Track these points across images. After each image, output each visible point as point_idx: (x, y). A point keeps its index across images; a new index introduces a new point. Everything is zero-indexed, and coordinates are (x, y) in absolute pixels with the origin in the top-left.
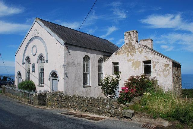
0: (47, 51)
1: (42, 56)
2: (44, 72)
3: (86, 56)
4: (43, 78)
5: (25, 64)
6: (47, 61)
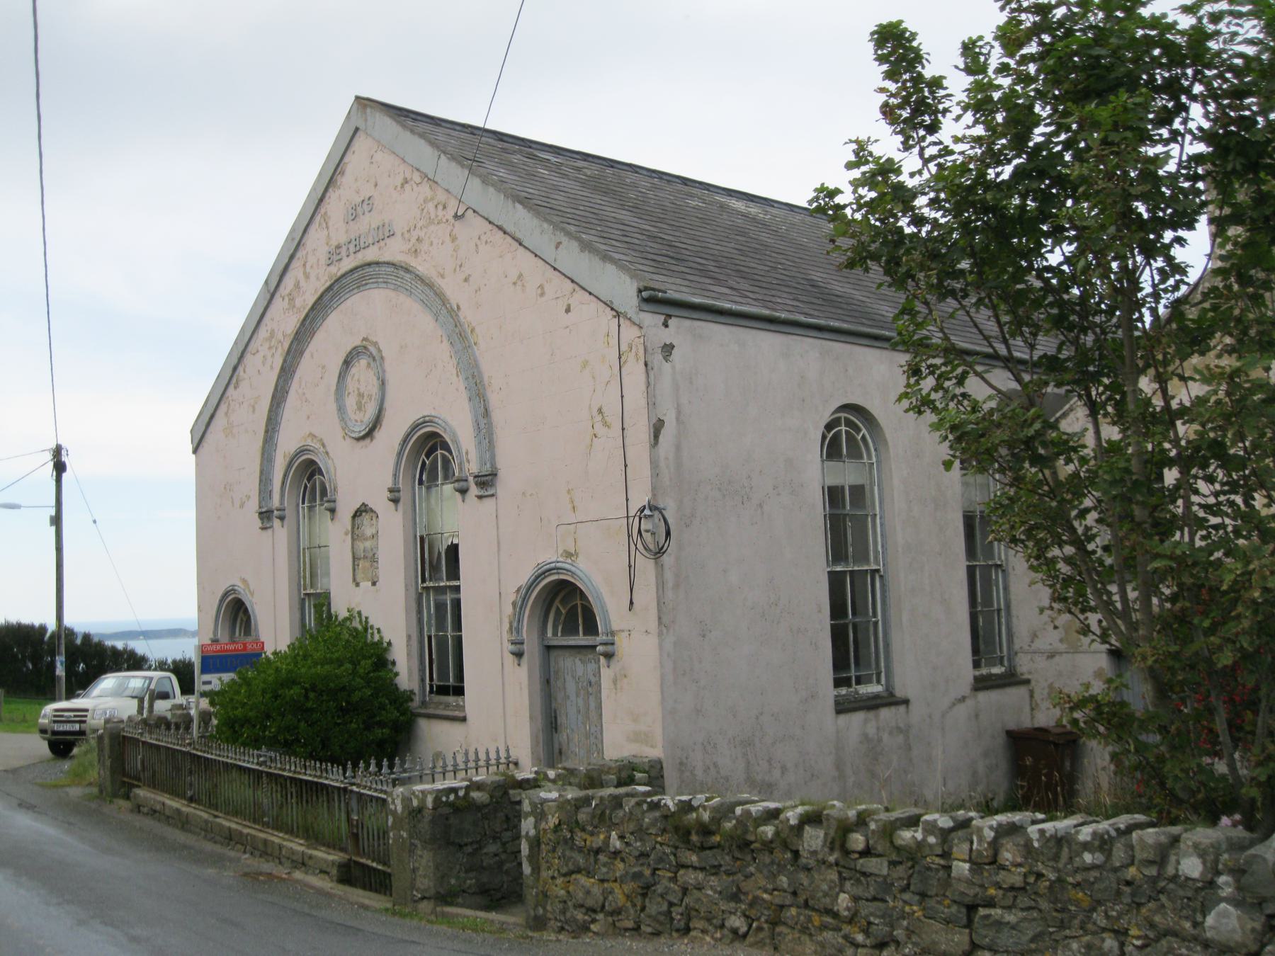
0: (478, 393)
1: (434, 435)
2: (464, 582)
3: (846, 407)
4: (459, 642)
5: (282, 518)
6: (487, 481)
